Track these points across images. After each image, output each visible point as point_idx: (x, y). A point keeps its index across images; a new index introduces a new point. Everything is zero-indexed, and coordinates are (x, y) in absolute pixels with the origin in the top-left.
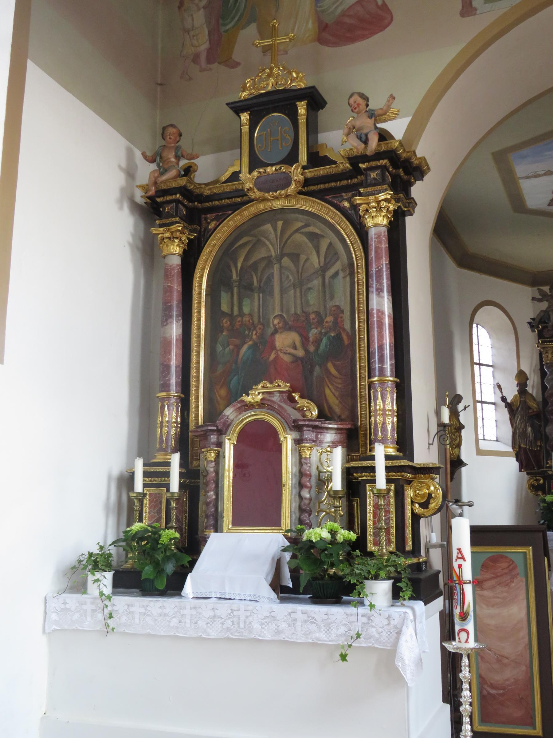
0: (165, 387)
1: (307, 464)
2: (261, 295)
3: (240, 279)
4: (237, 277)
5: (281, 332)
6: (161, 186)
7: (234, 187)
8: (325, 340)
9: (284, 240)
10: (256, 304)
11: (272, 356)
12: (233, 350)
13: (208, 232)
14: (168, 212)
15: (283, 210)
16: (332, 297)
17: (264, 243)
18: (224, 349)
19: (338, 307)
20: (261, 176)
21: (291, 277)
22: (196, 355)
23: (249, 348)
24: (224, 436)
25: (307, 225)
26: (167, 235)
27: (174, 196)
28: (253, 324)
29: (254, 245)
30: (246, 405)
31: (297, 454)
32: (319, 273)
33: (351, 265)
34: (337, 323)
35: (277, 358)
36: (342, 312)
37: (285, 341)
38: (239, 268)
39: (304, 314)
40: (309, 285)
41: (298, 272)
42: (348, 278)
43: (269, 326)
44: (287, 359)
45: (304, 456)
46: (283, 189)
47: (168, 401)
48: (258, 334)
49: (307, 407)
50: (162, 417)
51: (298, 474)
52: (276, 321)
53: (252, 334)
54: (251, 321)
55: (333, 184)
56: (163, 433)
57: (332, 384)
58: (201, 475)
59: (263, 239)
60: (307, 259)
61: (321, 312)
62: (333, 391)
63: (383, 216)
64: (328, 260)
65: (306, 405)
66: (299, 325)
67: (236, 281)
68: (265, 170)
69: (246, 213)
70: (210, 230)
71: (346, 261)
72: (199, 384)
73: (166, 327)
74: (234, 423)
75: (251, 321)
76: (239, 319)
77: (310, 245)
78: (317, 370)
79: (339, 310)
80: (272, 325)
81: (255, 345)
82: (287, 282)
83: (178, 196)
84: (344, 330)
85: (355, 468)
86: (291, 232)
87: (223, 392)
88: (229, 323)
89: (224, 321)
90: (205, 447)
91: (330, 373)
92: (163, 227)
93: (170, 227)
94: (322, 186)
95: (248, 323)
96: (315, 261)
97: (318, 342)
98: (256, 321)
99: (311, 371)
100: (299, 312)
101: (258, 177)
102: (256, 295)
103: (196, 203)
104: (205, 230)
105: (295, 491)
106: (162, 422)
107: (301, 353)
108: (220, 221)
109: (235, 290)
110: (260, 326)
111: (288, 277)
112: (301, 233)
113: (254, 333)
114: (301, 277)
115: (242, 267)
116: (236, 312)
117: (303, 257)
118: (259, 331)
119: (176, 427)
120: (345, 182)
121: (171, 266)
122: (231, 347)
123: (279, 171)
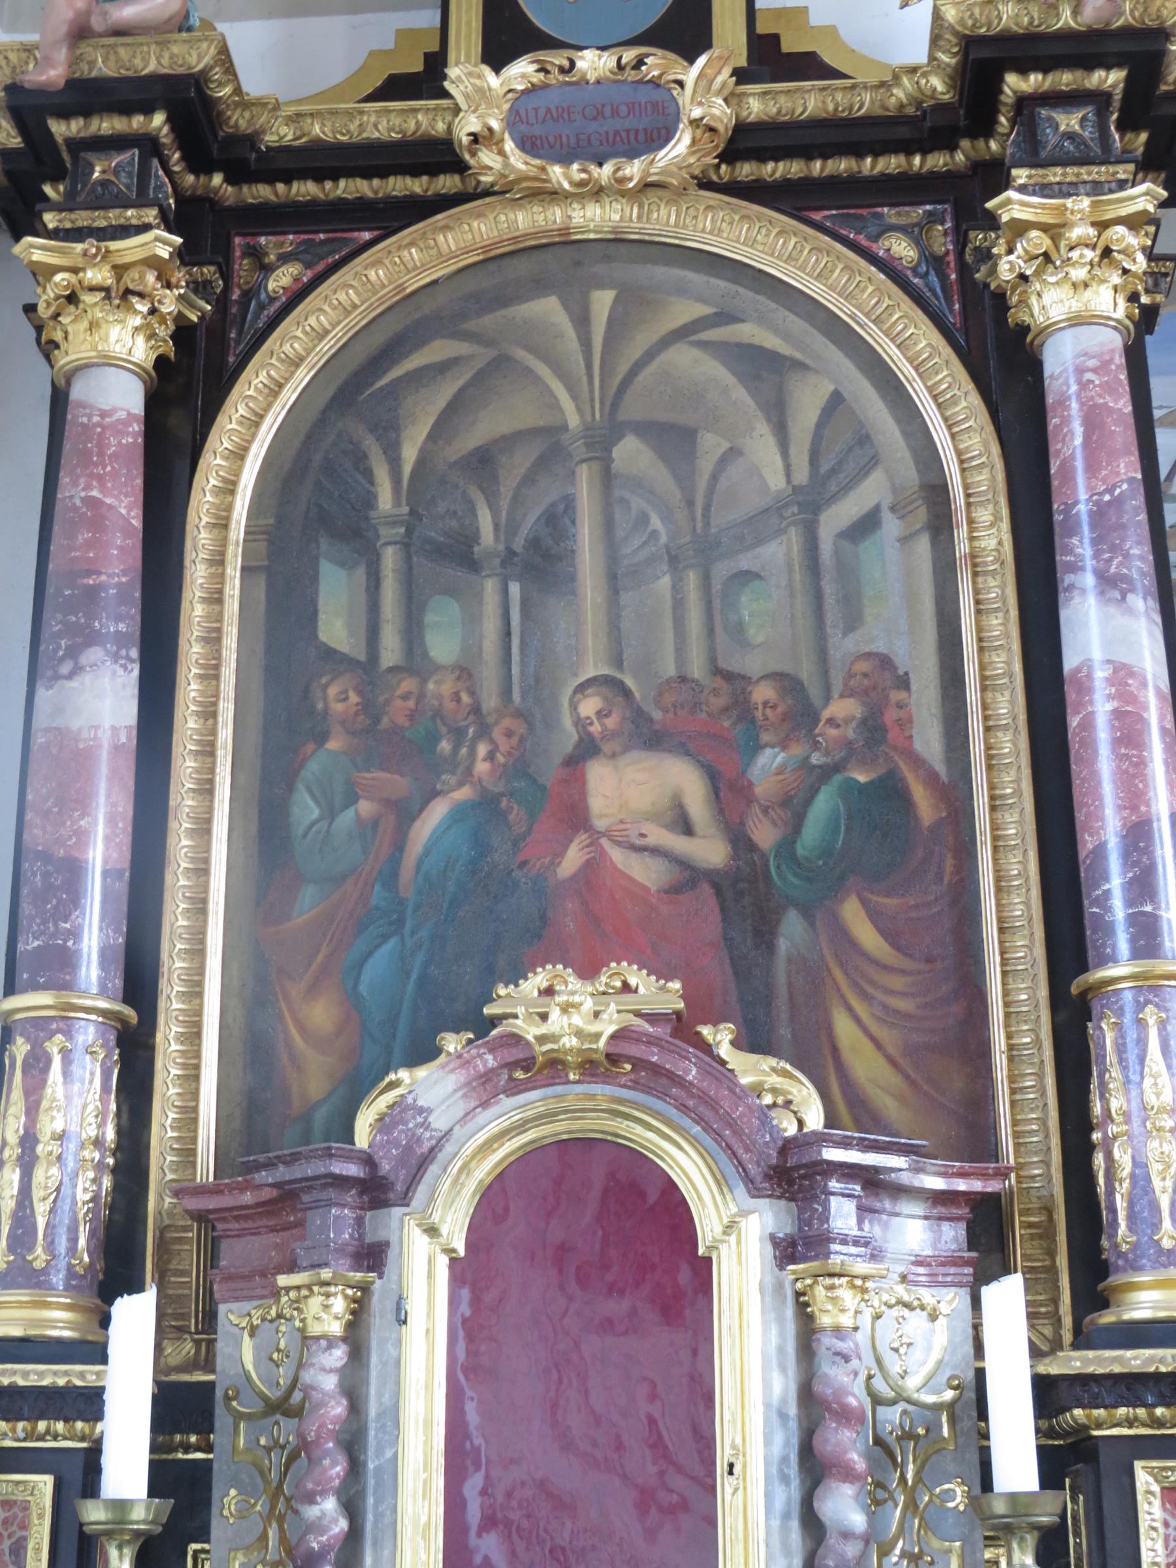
0: (57, 966)
1: (847, 1359)
2: (515, 589)
3: (413, 512)
4: (397, 502)
5: (614, 756)
6: (92, 63)
7: (412, 125)
8: (824, 804)
9: (623, 368)
10: (491, 627)
11: (573, 858)
12: (375, 824)
13: (262, 307)
14: (104, 183)
15: (616, 244)
16: (853, 621)
17: (529, 371)
18: (331, 813)
19: (885, 662)
20: (545, 86)
21: (656, 522)
22: (191, 833)
23: (458, 815)
24: (397, 1211)
25: (724, 318)
26: (97, 275)
27: (137, 121)
28: (476, 710)
29: (479, 378)
30: (527, 1064)
31: (790, 1311)
32: (787, 513)
33: (936, 493)
34: (883, 729)
35: (593, 867)
36: (904, 683)
37: (636, 793)
38: (407, 469)
39: (719, 682)
40: (745, 562)
41: (690, 503)
42: (923, 546)
43: (551, 723)
44: (646, 873)
45: (825, 1320)
46: (631, 155)
47: (68, 1034)
48: (500, 759)
49: (774, 1091)
50: (32, 1110)
51: (793, 1410)
52: (589, 707)
53: (472, 753)
54: (465, 698)
55: (842, 165)
56: (37, 1194)
57: (865, 996)
58: (219, 1410)
59: (521, 354)
60: (733, 453)
61: (804, 676)
62: (874, 1028)
63: (1115, 289)
64: (824, 468)
65: (775, 1080)
66: (710, 721)
67: (393, 522)
68: (572, 64)
69: (449, 241)
70: (272, 300)
71: (910, 475)
72: (201, 971)
73: (74, 684)
74: (449, 1148)
75: (465, 698)
76: (408, 684)
77: (740, 393)
78: (792, 932)
79: (883, 678)
80: (567, 722)
81: (487, 806)
82: (636, 543)
83: (159, 119)
84: (917, 762)
85: (1084, 1380)
86: (655, 337)
87: (322, 1014)
88: (354, 698)
89: (332, 691)
90: (292, 1267)
91: (854, 944)
92: (81, 241)
93: (114, 245)
94: (794, 169)
95: (450, 705)
96: (768, 467)
97: (794, 806)
98: (490, 701)
99: (764, 934)
100: (697, 669)
101: (533, 89)
102: (490, 586)
103: (217, 179)
104: (247, 295)
105: (789, 1494)
106: (29, 1140)
107: (710, 851)
108: (320, 267)
109: (390, 558)
110: (506, 722)
111: (643, 519)
112: (704, 345)
113: (482, 749)
114: (707, 524)
115: (421, 463)
116: (391, 650)
117: (711, 445)
118: (504, 745)
119: (100, 1166)
120: (892, 163)
121: (104, 414)
122: (365, 807)
123: (630, 75)
